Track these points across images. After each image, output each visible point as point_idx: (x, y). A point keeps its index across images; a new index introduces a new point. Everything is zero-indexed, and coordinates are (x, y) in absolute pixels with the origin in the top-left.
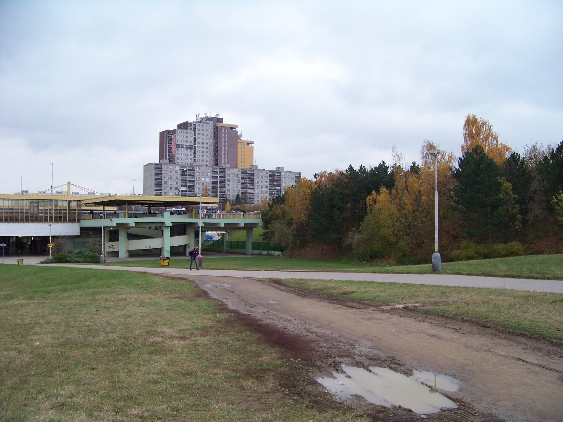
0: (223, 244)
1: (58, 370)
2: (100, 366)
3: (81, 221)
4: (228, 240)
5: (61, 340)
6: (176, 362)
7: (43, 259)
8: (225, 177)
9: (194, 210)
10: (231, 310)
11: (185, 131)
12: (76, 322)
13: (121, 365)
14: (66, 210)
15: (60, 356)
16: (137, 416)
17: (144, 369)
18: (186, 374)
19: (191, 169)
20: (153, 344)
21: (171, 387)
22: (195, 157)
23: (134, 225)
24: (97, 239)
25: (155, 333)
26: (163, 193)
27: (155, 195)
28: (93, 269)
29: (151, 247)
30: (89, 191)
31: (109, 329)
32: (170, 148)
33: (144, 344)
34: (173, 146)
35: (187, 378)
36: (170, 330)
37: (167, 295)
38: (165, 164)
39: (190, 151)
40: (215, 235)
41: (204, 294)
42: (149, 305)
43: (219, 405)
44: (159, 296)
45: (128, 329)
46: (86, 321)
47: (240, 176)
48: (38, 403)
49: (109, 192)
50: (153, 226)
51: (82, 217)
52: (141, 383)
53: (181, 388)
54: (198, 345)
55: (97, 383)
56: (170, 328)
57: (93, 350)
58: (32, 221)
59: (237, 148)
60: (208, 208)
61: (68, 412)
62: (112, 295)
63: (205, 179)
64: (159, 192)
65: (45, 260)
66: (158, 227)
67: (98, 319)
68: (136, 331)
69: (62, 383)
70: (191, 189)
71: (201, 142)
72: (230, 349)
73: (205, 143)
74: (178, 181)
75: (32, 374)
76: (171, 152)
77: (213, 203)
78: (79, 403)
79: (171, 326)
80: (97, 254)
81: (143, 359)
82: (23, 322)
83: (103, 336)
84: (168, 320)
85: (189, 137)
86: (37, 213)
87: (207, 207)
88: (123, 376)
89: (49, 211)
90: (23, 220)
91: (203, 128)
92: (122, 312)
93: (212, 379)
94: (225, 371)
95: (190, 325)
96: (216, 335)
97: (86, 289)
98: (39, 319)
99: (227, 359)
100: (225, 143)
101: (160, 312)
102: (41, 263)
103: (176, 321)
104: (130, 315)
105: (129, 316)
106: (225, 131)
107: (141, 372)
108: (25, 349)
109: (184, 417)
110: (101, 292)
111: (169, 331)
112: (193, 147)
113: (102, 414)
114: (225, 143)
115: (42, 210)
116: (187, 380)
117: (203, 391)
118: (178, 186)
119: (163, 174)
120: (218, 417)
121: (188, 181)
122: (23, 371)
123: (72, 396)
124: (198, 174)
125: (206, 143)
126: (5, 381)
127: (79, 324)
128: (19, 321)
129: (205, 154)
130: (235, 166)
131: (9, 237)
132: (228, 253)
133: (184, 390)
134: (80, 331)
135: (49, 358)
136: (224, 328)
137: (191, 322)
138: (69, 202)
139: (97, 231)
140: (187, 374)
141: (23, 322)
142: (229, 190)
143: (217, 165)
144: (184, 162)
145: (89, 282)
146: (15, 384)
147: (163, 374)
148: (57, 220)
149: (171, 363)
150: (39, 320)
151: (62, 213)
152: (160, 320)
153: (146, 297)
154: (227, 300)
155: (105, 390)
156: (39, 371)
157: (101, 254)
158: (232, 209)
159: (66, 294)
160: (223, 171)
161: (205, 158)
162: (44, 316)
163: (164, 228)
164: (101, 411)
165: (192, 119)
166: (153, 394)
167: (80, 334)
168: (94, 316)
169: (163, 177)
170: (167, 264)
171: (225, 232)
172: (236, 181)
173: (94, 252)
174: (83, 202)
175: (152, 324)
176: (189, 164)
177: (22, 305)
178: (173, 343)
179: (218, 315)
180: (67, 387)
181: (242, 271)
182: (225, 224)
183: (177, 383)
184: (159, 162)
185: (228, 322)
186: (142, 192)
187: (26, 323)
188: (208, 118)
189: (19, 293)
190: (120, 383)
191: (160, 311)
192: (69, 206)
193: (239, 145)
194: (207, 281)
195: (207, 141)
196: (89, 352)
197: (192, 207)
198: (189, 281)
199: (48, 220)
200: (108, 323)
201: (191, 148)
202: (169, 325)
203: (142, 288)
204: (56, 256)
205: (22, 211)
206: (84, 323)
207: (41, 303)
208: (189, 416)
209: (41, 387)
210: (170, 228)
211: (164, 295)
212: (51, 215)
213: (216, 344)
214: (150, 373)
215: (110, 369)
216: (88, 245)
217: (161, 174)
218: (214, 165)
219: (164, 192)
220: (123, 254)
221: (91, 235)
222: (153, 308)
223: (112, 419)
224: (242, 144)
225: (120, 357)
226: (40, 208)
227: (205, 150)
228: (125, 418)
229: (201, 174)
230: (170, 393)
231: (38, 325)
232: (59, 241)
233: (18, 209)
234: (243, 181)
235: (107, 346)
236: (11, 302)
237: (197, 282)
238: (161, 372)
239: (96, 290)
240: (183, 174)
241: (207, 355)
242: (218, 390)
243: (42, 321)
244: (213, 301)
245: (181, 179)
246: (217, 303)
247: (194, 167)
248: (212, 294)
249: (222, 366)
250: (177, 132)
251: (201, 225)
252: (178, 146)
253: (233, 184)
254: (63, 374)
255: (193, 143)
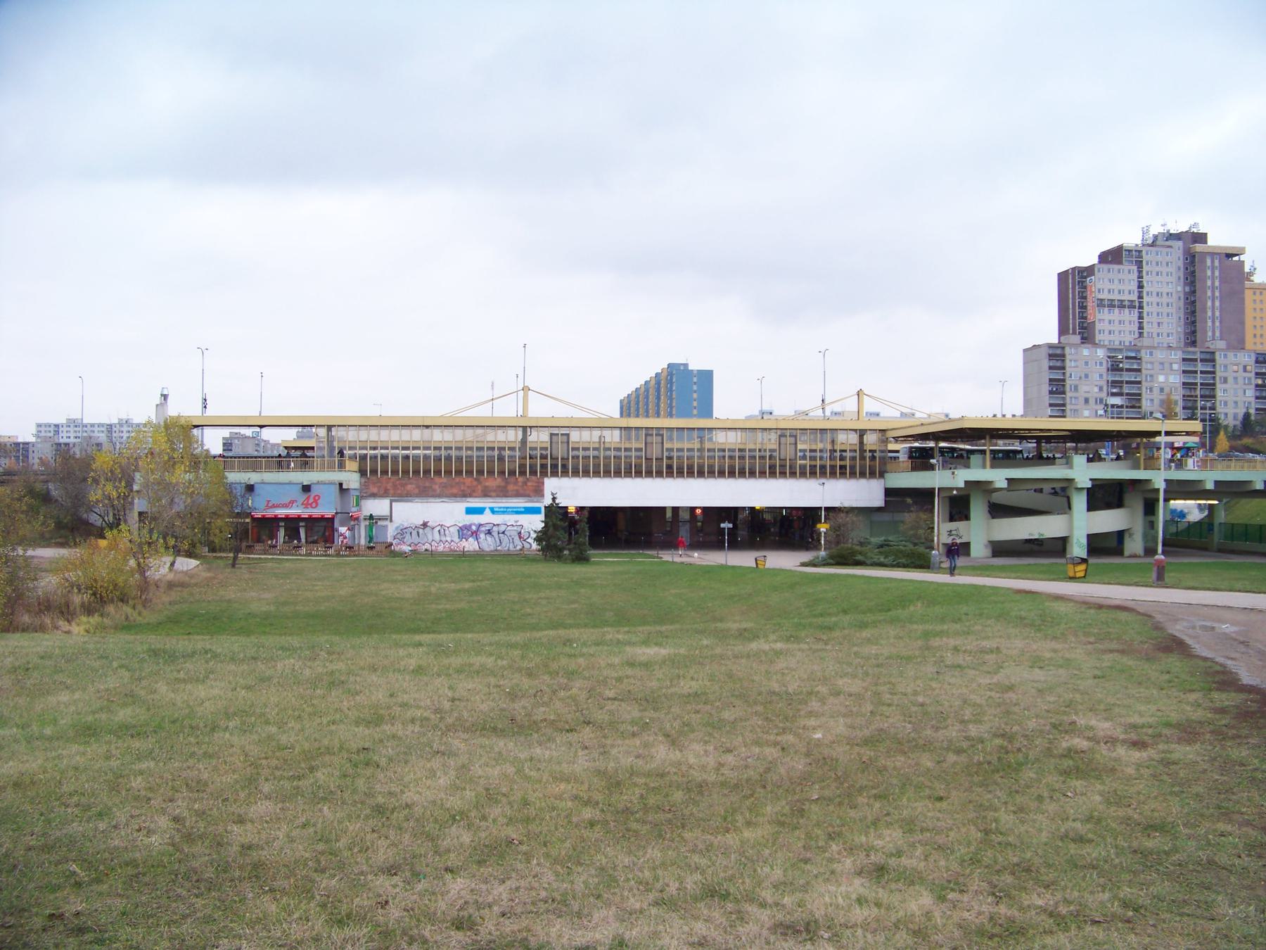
0: (1212, 530)
1: (865, 794)
2: (954, 793)
3: (887, 475)
4: (1223, 521)
5: (866, 731)
6: (1125, 797)
7: (806, 556)
8: (1214, 373)
9: (1142, 451)
10: (1247, 685)
11: (1116, 267)
12: (895, 694)
13: (1000, 795)
14: (855, 451)
15: (865, 766)
16: (1043, 910)
17: (1051, 807)
18: (1151, 828)
19: (1133, 355)
20: (1070, 753)
21: (1117, 855)
22: (1141, 328)
23: (1004, 485)
24: (923, 516)
25: (1072, 729)
26: (1068, 413)
27: (1050, 416)
28: (917, 581)
29: (1042, 535)
30: (905, 410)
31: (968, 713)
32: (1083, 307)
33: (1049, 752)
34: (1090, 304)
35: (1154, 837)
36: (1107, 725)
37: (1090, 643)
38: (1071, 345)
39: (1130, 313)
40: (1191, 509)
41: (1176, 646)
42: (1054, 665)
43: (1237, 910)
44: (1072, 645)
45: (1010, 716)
46: (915, 693)
47: (1252, 367)
48: (831, 860)
49: (946, 412)
50: (1047, 488)
51: (889, 467)
52: (1048, 837)
53: (1141, 858)
54: (1174, 763)
55: (951, 829)
56: (1106, 719)
57: (937, 759)
58: (783, 474)
59: (1242, 301)
60: (1176, 445)
61: (893, 886)
62: (966, 639)
63: (1167, 379)
64: (1060, 409)
65: (812, 558)
66: (1058, 490)
67: (943, 692)
68: (1029, 723)
69: (875, 823)
70: (1134, 402)
71: (1155, 290)
72: (1254, 779)
73: (1165, 295)
74: (1104, 384)
75: (813, 798)
76: (1086, 318)
77: (1188, 434)
78: (914, 869)
79: (1108, 712)
80: (921, 549)
81: (1048, 785)
82: (784, 689)
83: (956, 728)
84: (1100, 702)
85: (1126, 281)
86: (793, 457)
87: (1173, 443)
88: (1006, 818)
89: (818, 454)
90: (765, 473)
91: (1159, 258)
92: (992, 678)
93: (1214, 846)
94: (1244, 829)
95: (1152, 716)
96: (1216, 743)
97: (907, 624)
98: (816, 683)
99: (1249, 800)
100: (1213, 292)
101: (1079, 682)
102: (803, 565)
103: (1119, 705)
104: (1013, 685)
105: (1011, 688)
106: (1213, 262)
107: (1046, 815)
108: (793, 745)
109: (1154, 926)
110: (942, 632)
111: (1103, 727)
112: (1137, 305)
113: (965, 898)
114: (1213, 292)
115: (804, 451)
116: (1154, 842)
117: (1194, 870)
118: (1104, 395)
119: (1067, 369)
120: (1239, 938)
121: (1127, 382)
122: (794, 790)
123: (899, 854)
124: (1149, 366)
125: (1168, 294)
126: (762, 807)
127: (901, 699)
128: (776, 687)
129: (1165, 320)
130: (1239, 345)
131: (736, 510)
132: (1222, 550)
133: (1149, 864)
134: (905, 716)
135: (846, 768)
136: (1233, 727)
137: (1153, 708)
138: (862, 433)
139: (924, 497)
140: (1153, 827)
141: (784, 689)
142: (1226, 403)
143: (1194, 343)
144: (1116, 340)
145: (912, 608)
146: (782, 816)
147: (1096, 823)
148: (836, 473)
149: (1115, 799)
150: (817, 686)
151: (846, 457)
152: (1081, 701)
153: (1044, 647)
154: (1234, 663)
155: (969, 847)
156: (827, 793)
157: (933, 548)
158: (1232, 448)
159: (866, 634)
160: (1210, 358)
161: (1165, 329)
162: (825, 679)
163: (1073, 490)
164: (963, 891)
165: (1132, 239)
166: (1076, 866)
167: (905, 721)
168: (934, 685)
169: (1068, 375)
170: (1082, 574)
171: (1216, 502)
172: (1240, 381)
173: (915, 544)
174: (891, 434)
175: (1063, 708)
176: (1127, 344)
177: (778, 653)
178: (1114, 754)
179: (1216, 695)
180: (887, 832)
181: (1262, 595)
182: (1217, 483)
183: (1129, 847)
184: (1057, 342)
185: (1244, 715)
186: (1019, 411)
187: (790, 690)
188: (1171, 234)
189: (768, 627)
190: (1001, 834)
191: (1078, 679)
192: (861, 442)
193: (1248, 294)
194: (1180, 616)
195: (1170, 289)
196: (927, 762)
197: (1138, 444)
198: (1139, 613)
199: (816, 473)
200: (965, 702)
201: (1132, 306)
202: (1103, 713)
203: (1032, 625)
204: (834, 550)
205: (762, 453)
206: (913, 697)
207: (817, 650)
208: (1165, 926)
209: (833, 827)
210: (1085, 492)
211: (1085, 644)
212: (823, 463)
213: (1217, 764)
214: (1067, 819)
215: (977, 801)
216: (902, 528)
217: (1064, 368)
218: (1186, 345)
219: (1071, 410)
220: (979, 550)
221: (909, 505)
222: (1061, 671)
223: (990, 912)
224: (1255, 293)
225: (997, 776)
226: (800, 447)
227: (1165, 310)
228: (1016, 913)
229: (1157, 366)
230: (1115, 867)
231: (816, 696)
232: (841, 518)
233: (755, 450)
234: (1260, 382)
235: (965, 751)
236: (754, 646)
237: (1159, 617)
238: (1092, 817)
239: (931, 627)
240: (1115, 368)
241: (1199, 789)
242: (1231, 872)
243: (824, 689)
244: (1201, 663)
245: (1110, 379)
246: (1210, 667)
247: (1139, 351)
248: (1197, 646)
249: (1236, 817)
250: (1099, 271)
251: (1161, 485)
252: (1101, 304)
253: (1235, 389)
254: (877, 805)
255: (1136, 294)
